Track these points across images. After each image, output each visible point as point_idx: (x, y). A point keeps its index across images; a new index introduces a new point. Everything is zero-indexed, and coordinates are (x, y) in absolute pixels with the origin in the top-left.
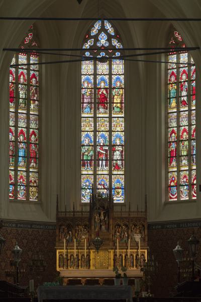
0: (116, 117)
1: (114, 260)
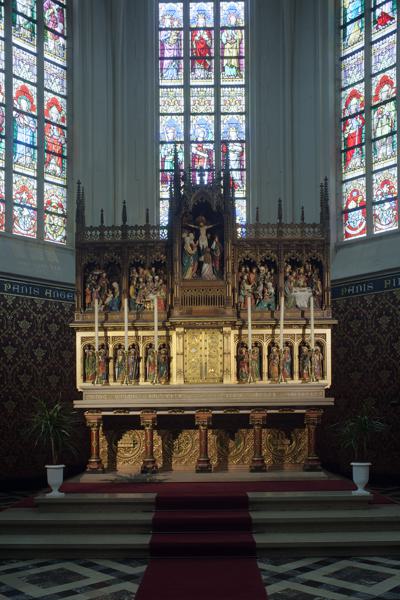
0: (228, 86)
1: (237, 357)
